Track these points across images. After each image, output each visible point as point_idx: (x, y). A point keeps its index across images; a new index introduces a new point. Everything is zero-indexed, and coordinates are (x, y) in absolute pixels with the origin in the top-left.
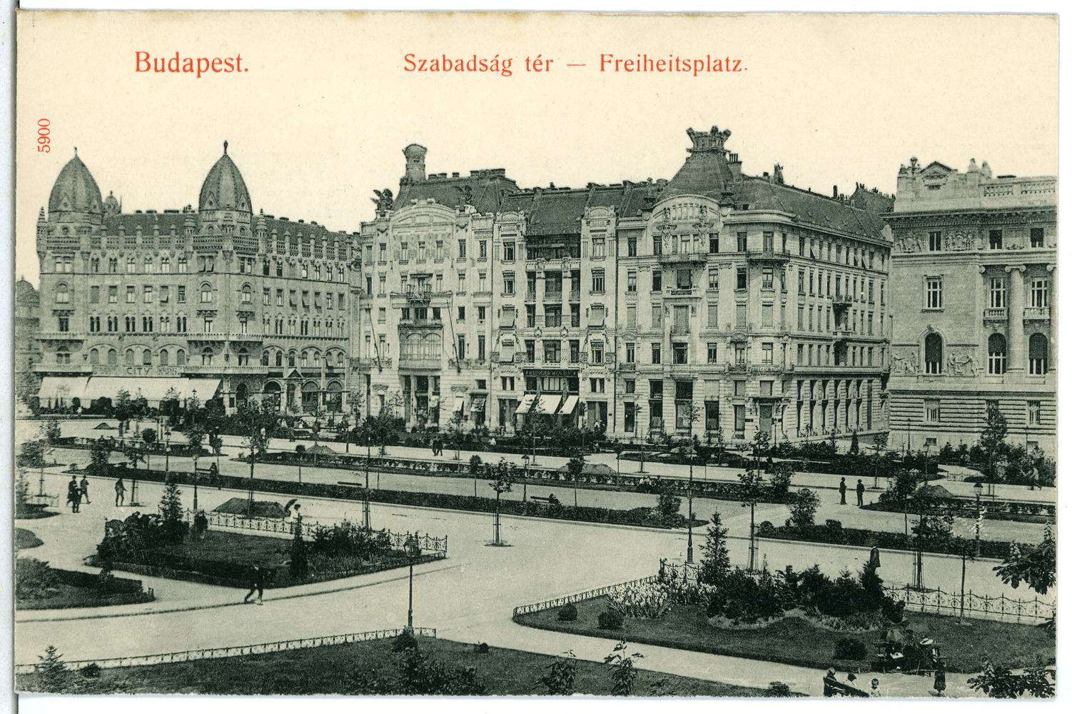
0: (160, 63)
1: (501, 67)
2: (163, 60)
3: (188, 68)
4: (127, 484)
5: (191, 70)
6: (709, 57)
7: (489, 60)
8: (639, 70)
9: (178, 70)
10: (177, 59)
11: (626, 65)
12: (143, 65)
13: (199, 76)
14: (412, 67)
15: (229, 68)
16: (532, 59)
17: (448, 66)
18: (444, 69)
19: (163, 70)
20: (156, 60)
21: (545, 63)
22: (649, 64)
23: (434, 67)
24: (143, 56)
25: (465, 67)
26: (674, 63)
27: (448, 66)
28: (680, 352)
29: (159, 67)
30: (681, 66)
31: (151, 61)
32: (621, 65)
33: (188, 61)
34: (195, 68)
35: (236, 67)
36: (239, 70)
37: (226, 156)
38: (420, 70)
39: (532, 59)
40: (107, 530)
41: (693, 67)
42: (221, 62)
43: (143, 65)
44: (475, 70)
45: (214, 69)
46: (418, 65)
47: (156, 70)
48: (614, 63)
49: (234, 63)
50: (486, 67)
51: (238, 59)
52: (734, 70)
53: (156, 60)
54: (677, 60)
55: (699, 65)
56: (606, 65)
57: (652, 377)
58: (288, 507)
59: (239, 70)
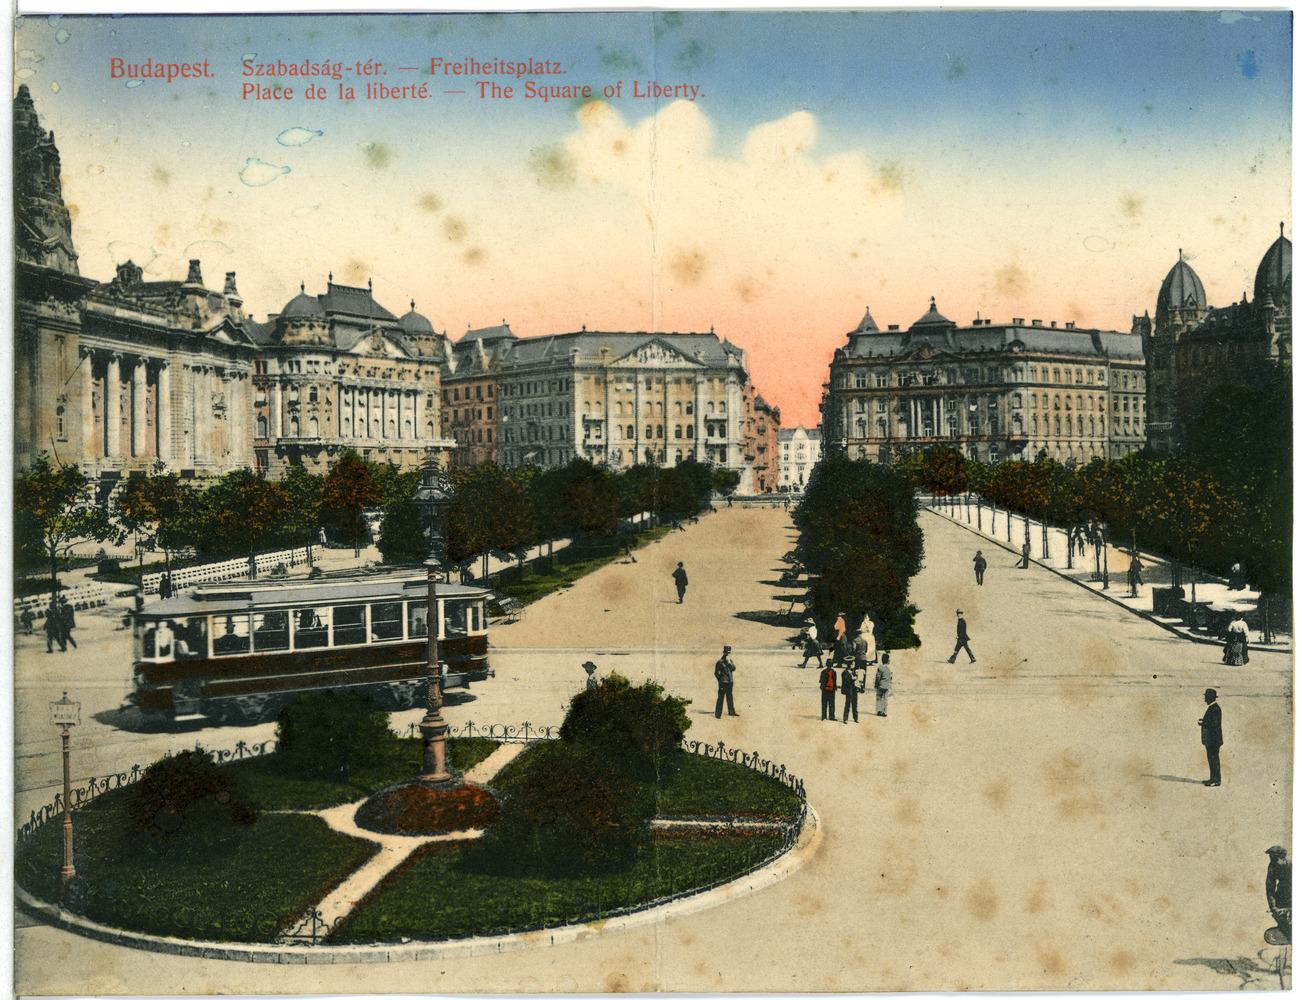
0: (133, 69)
1: (332, 72)
6: (531, 59)
7: (321, 65)
8: (558, 88)
10: (149, 65)
11: (454, 67)
18: (382, 97)
20: (129, 66)
21: (402, 91)
22: (475, 67)
25: (299, 71)
26: (499, 67)
27: (283, 69)
30: (506, 69)
31: (125, 67)
32: (450, 68)
33: (160, 67)
34: (166, 73)
38: (257, 74)
39: (363, 63)
41: (310, 69)
42: (189, 68)
43: (118, 72)
44: (308, 74)
46: (256, 70)
48: (443, 67)
49: (202, 68)
50: (194, 68)
51: (206, 65)
52: (555, 72)
53: (129, 66)
54: (502, 63)
56: (436, 68)
59: (206, 75)
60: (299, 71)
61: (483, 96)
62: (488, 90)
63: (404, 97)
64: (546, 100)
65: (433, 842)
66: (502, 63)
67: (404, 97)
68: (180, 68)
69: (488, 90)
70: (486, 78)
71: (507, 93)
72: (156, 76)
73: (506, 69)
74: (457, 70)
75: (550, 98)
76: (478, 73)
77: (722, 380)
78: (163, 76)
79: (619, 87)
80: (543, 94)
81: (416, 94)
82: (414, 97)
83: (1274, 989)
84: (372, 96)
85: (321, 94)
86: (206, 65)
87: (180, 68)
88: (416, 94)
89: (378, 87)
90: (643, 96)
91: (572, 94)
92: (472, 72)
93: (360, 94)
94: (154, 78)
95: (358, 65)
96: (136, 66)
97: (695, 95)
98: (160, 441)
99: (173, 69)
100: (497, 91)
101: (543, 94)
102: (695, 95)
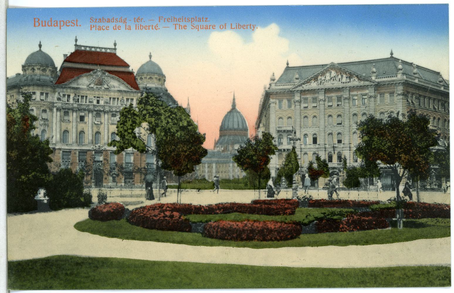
1: (123, 21)
2: (45, 21)
4: (241, 127)
12: (37, 24)
15: (73, 25)
17: (142, 27)
19: (45, 26)
26: (140, 27)
27: (142, 27)
28: (203, 167)
29: (44, 25)
30: (187, 20)
31: (40, 22)
33: (56, 22)
34: (59, 25)
35: (75, 24)
36: (77, 25)
37: (40, 50)
42: (69, 22)
47: (42, 26)
48: (163, 19)
51: (77, 21)
53: (42, 21)
55: (112, 21)
58: (269, 147)
59: (77, 25)
61: (176, 29)
62: (177, 26)
64: (198, 30)
65: (137, 209)
68: (65, 22)
69: (177, 26)
70: (175, 23)
71: (185, 27)
72: (54, 26)
73: (187, 20)
74: (146, 28)
75: (200, 29)
76: (176, 21)
77: (392, 94)
79: (225, 25)
80: (197, 28)
82: (153, 29)
84: (137, 28)
85: (119, 28)
86: (77, 21)
87: (65, 22)
89: (139, 25)
90: (234, 28)
91: (208, 28)
93: (133, 27)
94: (53, 27)
95: (135, 19)
99: (62, 23)
100: (181, 27)
101: (197, 28)
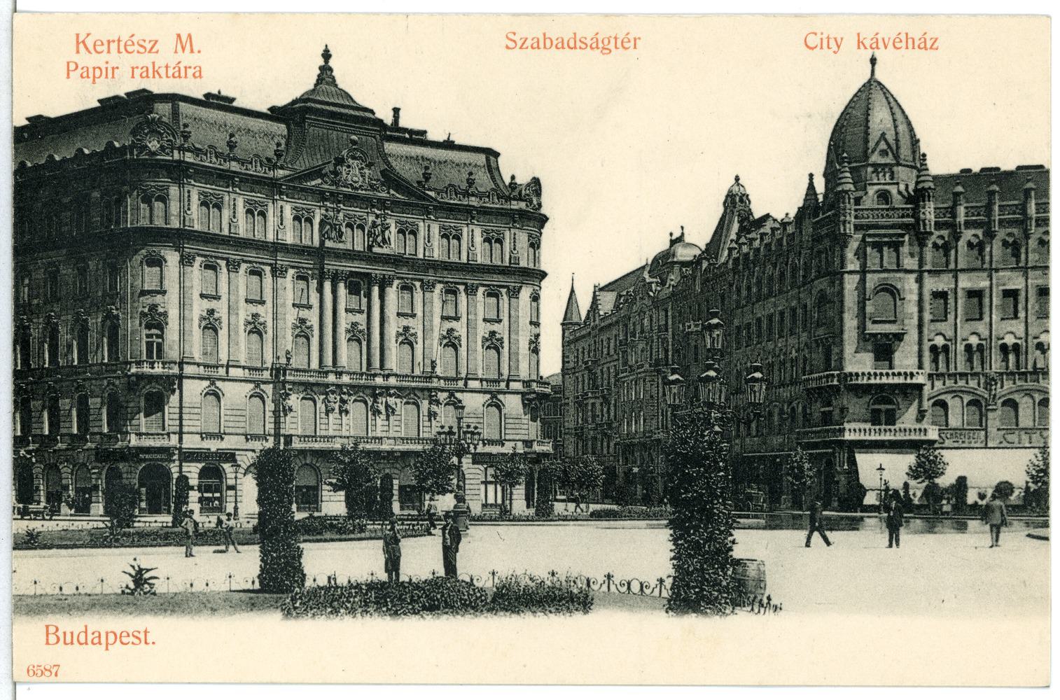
1: (601, 45)
2: (72, 633)
3: (96, 641)
5: (100, 643)
8: (907, 48)
9: (86, 643)
10: (86, 632)
12: (52, 639)
13: (107, 649)
14: (513, 45)
15: (137, 641)
16: (621, 36)
18: (545, 47)
20: (65, 633)
21: (106, 43)
22: (910, 41)
23: (535, 45)
24: (52, 630)
25: (566, 46)
29: (68, 639)
33: (96, 634)
34: (91, 75)
36: (146, 643)
38: (521, 48)
39: (621, 36)
40: (335, 599)
42: (128, 636)
43: (52, 639)
44: (575, 48)
45: (122, 643)
46: (519, 43)
47: (65, 643)
51: (146, 632)
52: (931, 48)
53: (65, 633)
57: (1023, 294)
59: (146, 643)
60: (566, 46)
63: (109, 52)
66: (828, 38)
67: (109, 52)
74: (898, 45)
78: (88, 77)
81: (122, 49)
83: (967, 314)
88: (122, 49)
91: (541, 45)
92: (782, 313)
96: (107, 77)
97: (839, 47)
98: (10, 68)
102: (839, 47)
